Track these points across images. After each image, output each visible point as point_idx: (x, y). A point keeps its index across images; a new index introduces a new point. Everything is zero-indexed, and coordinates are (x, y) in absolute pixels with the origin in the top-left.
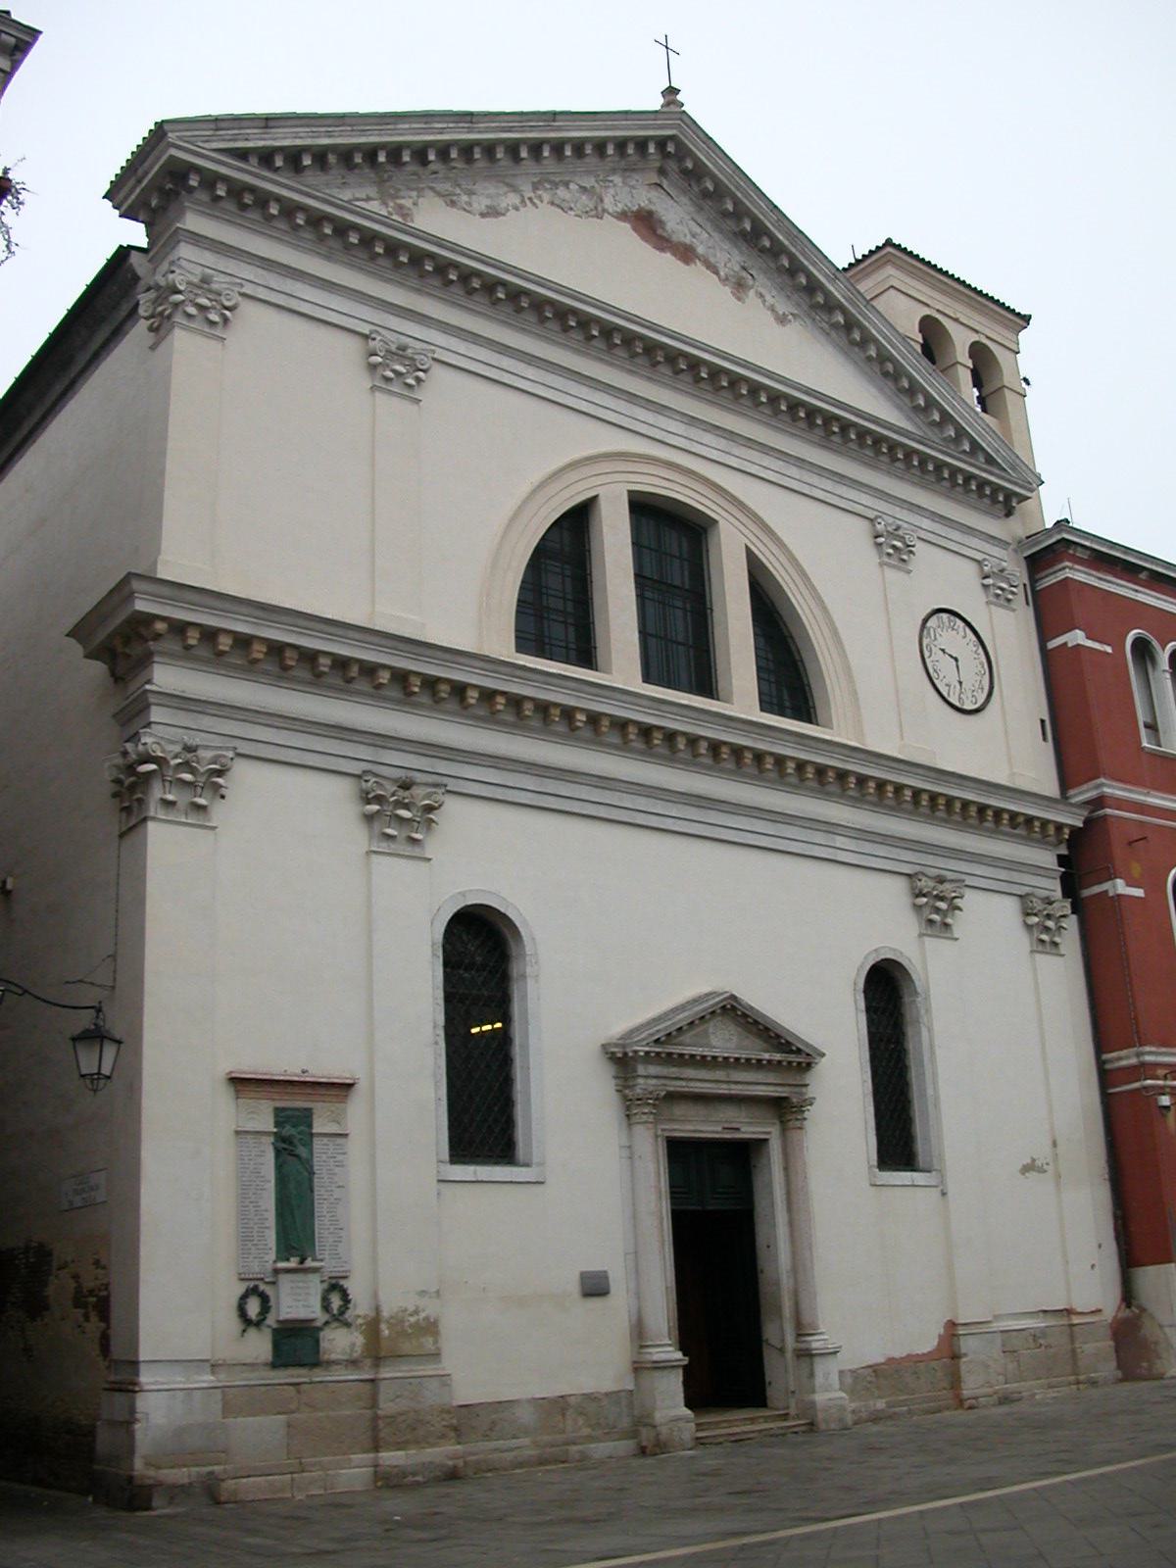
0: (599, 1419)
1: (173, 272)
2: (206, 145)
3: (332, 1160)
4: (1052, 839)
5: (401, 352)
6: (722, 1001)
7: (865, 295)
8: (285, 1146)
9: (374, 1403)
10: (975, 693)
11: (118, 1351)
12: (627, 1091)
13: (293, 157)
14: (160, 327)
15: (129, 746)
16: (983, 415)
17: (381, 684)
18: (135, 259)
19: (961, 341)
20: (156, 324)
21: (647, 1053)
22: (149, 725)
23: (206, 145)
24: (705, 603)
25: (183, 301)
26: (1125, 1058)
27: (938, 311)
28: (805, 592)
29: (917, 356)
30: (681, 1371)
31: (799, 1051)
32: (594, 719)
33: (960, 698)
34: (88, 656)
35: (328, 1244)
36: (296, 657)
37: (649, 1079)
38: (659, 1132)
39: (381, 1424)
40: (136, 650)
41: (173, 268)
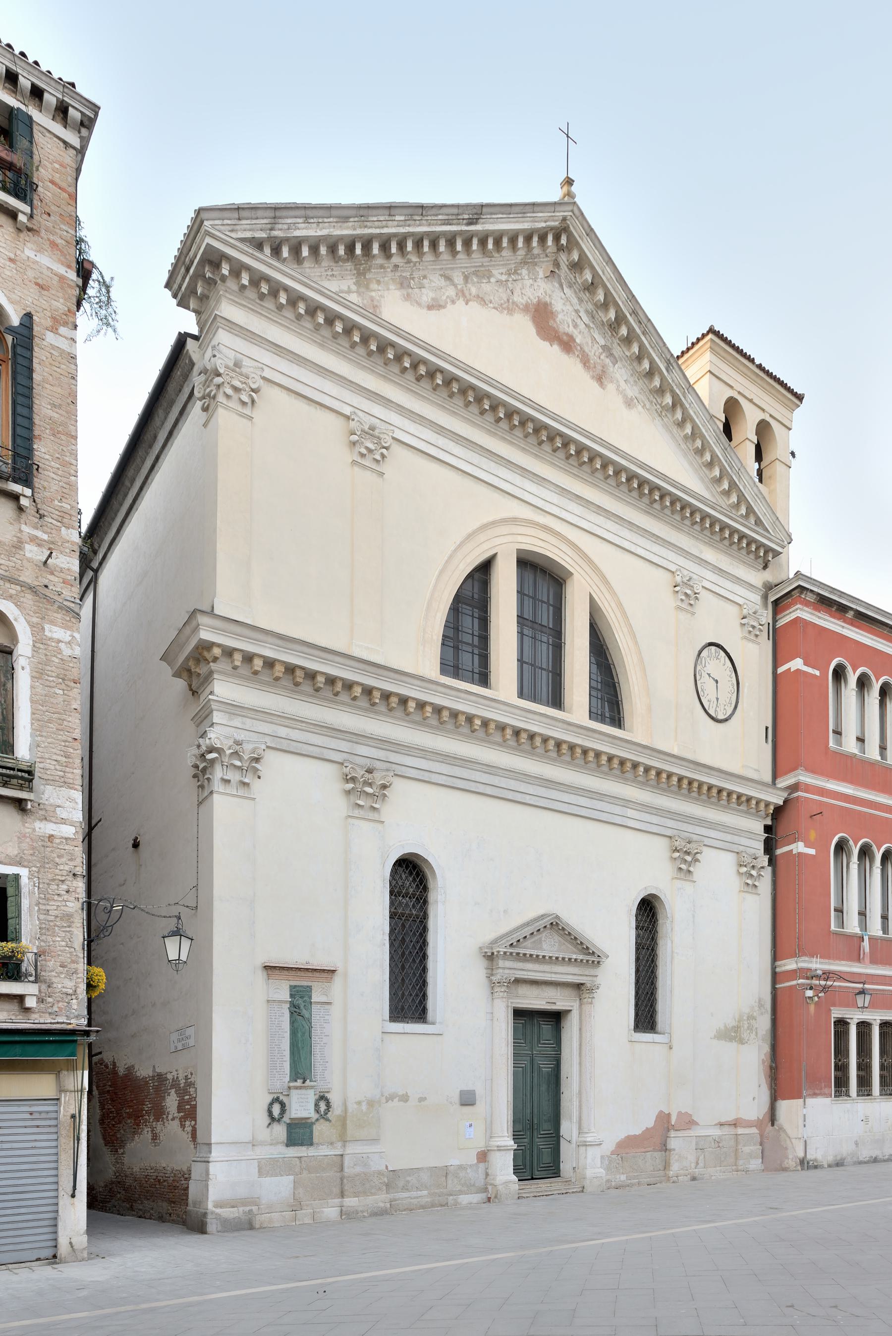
2: (233, 235)
6: (551, 920)
8: (295, 1009)
10: (726, 707)
17: (355, 696)
19: (751, 417)
21: (505, 953)
22: (212, 725)
23: (233, 235)
24: (561, 639)
27: (739, 393)
30: (512, 1152)
33: (716, 711)
36: (303, 676)
37: (508, 969)
38: (510, 1004)
40: (202, 670)
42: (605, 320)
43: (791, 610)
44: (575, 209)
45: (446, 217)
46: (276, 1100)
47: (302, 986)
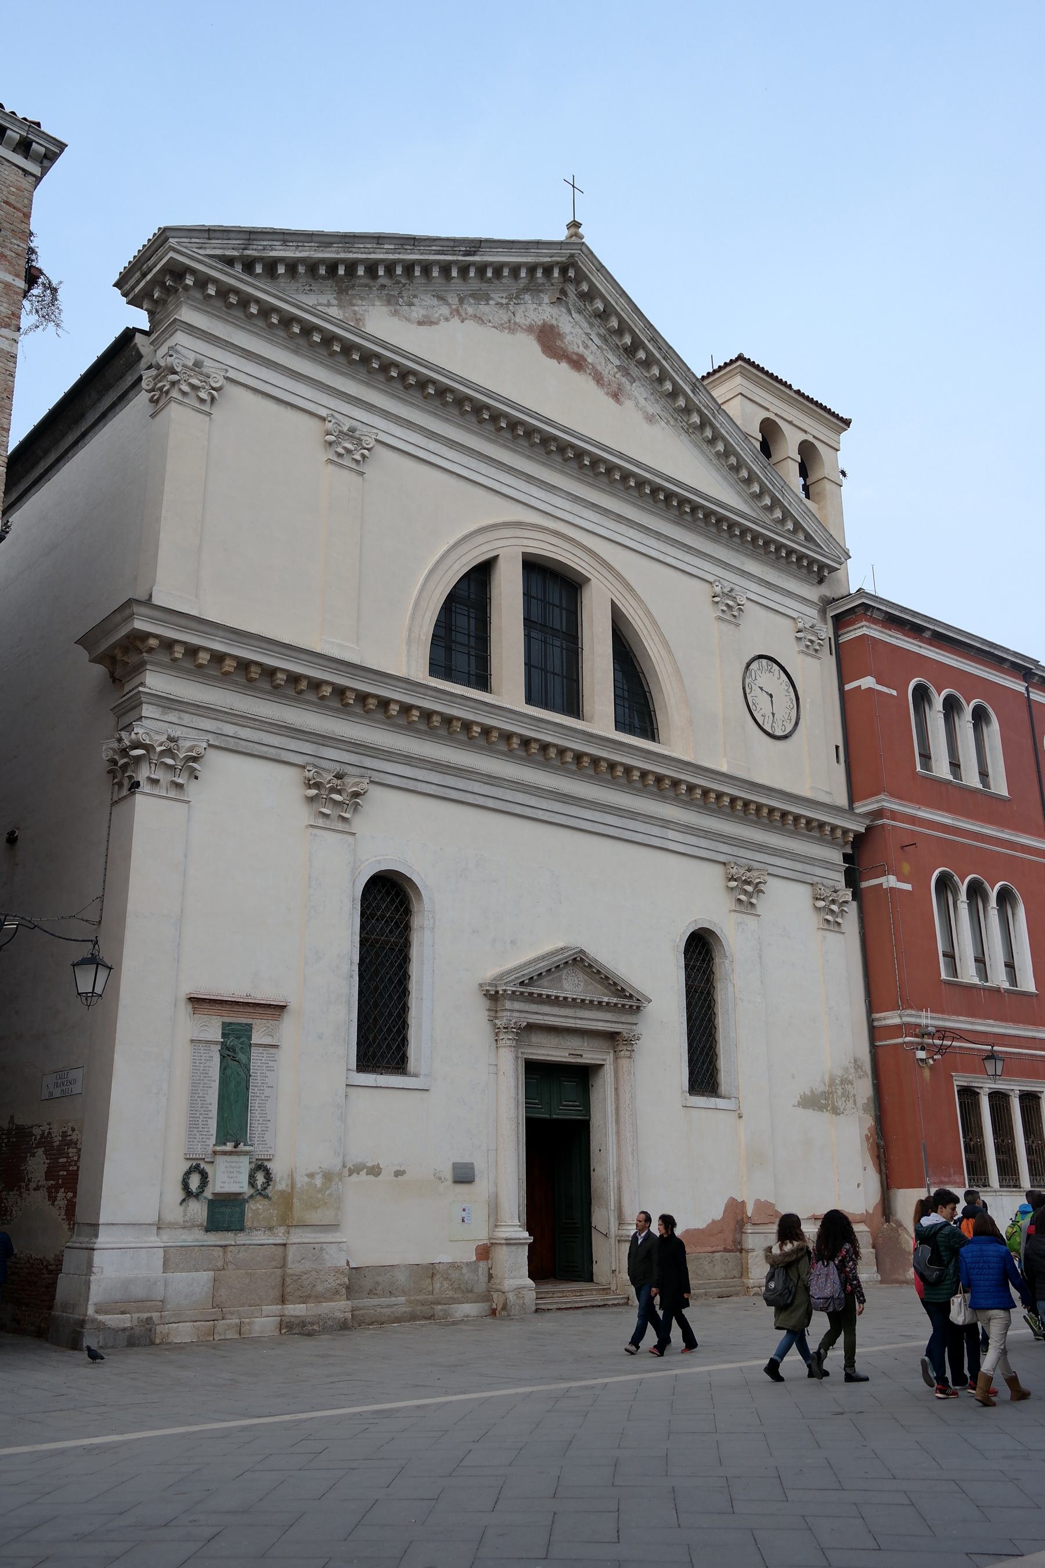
0: (460, 1284)
1: (171, 356)
2: (200, 251)
3: (265, 1065)
4: (840, 841)
5: (351, 433)
6: (574, 954)
7: (717, 399)
8: (228, 1052)
9: (284, 1266)
10: (785, 723)
11: (80, 1215)
12: (497, 1021)
13: (271, 265)
14: (158, 400)
15: (124, 734)
16: (806, 501)
17: (324, 696)
18: (139, 339)
20: (156, 397)
21: (514, 992)
25: (179, 381)
26: (891, 1018)
27: (776, 414)
28: (656, 638)
29: (756, 453)
30: (527, 1248)
31: (631, 996)
32: (487, 731)
34: (93, 660)
35: (256, 1136)
37: (517, 1013)
38: (520, 1055)
39: (288, 1280)
40: (133, 659)
41: (171, 352)
42: (619, 344)
43: (855, 627)
44: (584, 249)
45: (441, 248)
46: (196, 1169)
47: (239, 1024)
